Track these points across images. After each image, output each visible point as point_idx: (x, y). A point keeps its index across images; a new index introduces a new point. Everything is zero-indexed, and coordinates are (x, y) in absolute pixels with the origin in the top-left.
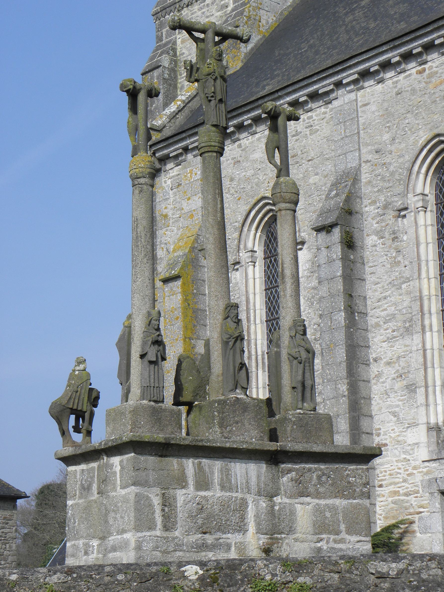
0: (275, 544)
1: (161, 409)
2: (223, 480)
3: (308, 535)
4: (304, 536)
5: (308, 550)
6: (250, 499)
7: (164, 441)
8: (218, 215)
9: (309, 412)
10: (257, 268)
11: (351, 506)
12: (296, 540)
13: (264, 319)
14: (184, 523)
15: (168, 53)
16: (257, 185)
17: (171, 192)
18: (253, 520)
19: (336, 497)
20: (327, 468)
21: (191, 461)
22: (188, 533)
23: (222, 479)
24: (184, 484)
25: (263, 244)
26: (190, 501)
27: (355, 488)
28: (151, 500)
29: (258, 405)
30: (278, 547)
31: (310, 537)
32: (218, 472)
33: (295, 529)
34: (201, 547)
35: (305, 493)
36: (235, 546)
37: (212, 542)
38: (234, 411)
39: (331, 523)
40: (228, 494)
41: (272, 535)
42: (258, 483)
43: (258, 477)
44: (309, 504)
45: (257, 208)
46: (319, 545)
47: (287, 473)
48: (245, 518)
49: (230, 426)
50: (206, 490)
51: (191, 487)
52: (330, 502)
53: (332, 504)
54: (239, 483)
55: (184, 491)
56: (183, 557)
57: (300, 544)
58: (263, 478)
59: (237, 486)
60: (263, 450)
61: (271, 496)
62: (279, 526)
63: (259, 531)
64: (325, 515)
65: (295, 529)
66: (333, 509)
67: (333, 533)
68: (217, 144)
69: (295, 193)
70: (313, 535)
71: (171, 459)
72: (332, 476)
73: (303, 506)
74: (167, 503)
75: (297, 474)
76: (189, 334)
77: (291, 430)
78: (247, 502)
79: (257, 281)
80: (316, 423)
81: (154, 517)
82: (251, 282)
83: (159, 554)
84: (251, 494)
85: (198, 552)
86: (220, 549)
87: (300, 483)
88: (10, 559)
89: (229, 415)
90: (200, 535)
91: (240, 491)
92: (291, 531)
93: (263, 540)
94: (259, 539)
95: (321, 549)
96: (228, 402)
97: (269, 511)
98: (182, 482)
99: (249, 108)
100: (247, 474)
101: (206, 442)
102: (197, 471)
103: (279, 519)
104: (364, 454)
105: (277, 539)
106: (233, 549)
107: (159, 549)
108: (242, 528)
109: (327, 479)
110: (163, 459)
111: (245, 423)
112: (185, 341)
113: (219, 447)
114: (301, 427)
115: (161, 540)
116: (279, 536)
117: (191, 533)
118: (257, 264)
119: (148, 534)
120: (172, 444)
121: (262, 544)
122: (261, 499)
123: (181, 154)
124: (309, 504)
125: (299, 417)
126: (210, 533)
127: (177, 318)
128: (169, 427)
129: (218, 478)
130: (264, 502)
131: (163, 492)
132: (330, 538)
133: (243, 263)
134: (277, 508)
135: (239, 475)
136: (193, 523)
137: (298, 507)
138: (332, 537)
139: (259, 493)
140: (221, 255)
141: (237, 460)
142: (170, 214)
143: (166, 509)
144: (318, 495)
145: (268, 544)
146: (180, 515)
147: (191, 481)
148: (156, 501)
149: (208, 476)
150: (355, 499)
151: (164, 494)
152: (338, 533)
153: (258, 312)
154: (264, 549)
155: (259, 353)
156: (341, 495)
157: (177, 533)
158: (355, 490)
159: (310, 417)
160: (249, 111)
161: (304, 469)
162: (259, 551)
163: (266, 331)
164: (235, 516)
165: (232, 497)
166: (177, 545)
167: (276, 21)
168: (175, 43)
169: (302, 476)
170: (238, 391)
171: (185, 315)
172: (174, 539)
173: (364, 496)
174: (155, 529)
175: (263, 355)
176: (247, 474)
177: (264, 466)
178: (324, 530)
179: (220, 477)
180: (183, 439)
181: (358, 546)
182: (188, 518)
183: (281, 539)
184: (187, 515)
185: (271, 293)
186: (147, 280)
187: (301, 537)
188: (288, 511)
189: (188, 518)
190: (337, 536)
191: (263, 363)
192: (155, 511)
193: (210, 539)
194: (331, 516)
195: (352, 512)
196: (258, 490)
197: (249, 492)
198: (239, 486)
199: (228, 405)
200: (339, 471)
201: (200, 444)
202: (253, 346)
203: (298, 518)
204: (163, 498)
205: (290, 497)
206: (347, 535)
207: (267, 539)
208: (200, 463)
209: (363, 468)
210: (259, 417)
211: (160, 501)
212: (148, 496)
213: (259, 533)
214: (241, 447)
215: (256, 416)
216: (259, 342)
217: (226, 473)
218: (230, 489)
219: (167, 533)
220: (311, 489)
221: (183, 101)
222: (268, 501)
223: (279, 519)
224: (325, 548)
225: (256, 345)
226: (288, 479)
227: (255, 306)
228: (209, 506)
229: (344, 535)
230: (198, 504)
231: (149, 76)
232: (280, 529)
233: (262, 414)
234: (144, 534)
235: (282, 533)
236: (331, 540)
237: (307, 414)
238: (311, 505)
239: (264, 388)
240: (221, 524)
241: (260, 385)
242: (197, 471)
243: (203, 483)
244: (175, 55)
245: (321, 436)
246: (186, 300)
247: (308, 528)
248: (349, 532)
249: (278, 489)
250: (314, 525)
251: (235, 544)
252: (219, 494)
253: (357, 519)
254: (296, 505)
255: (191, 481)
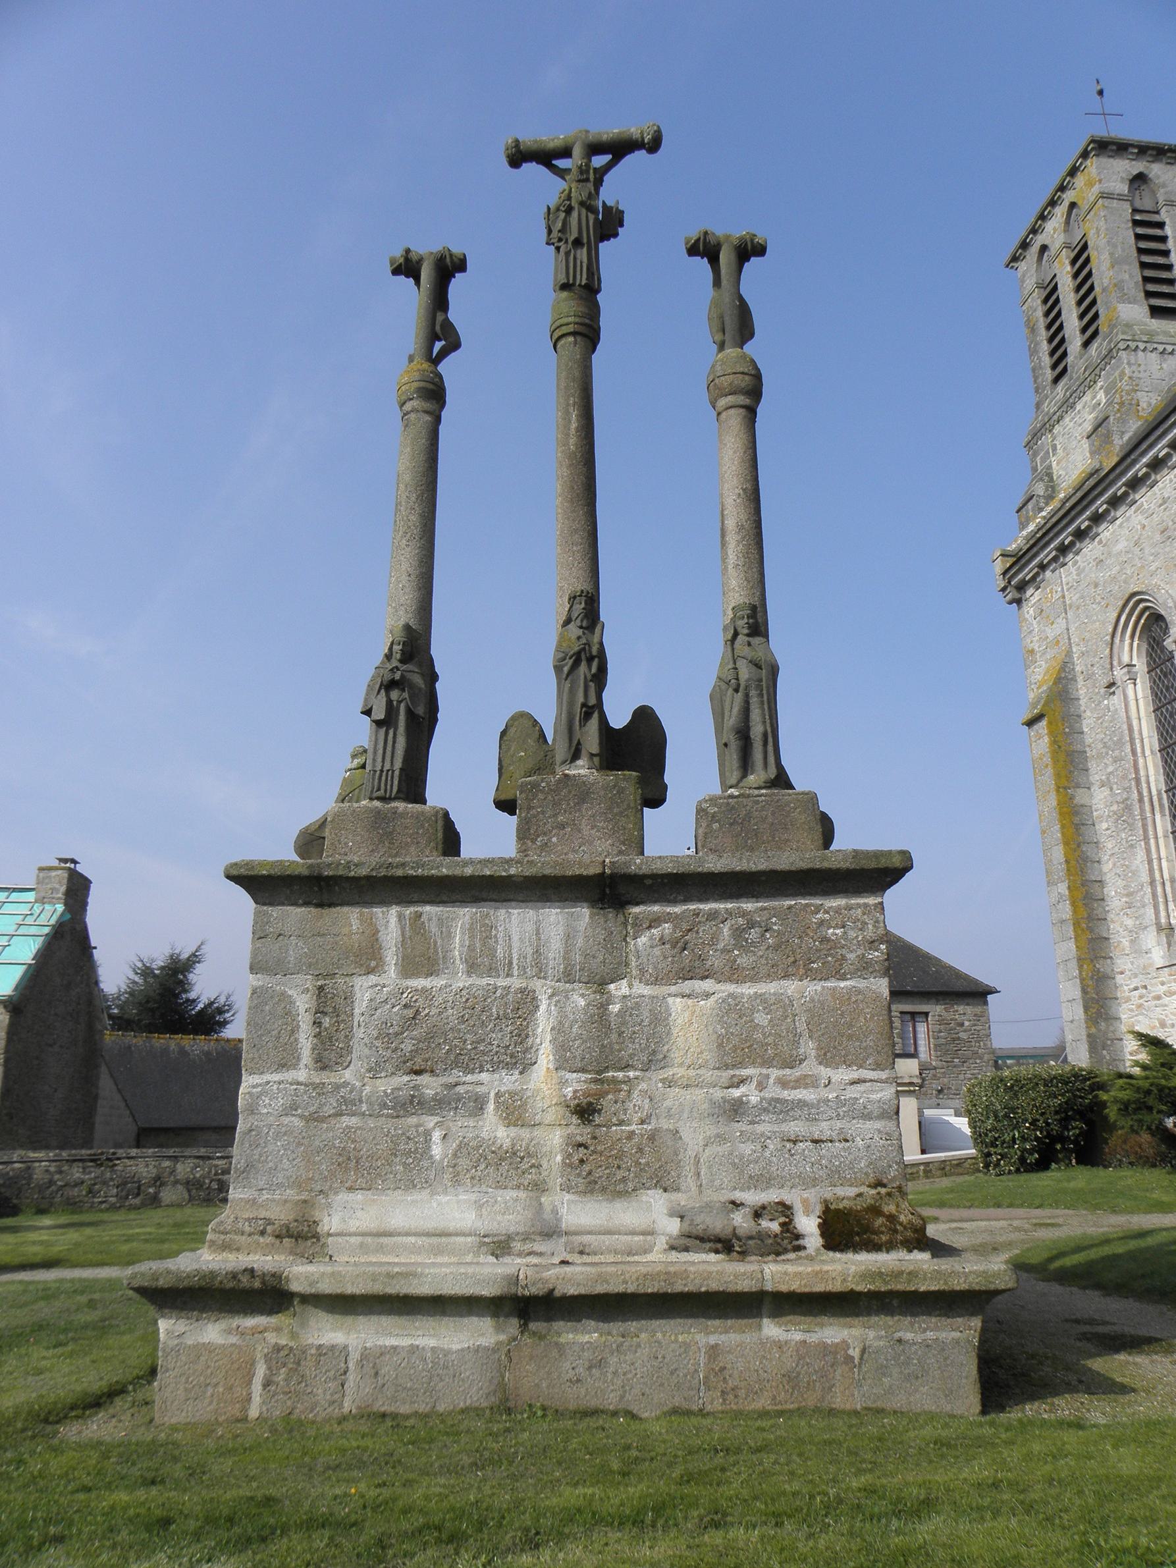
0: (607, 1093)
1: (395, 813)
2: (474, 950)
3: (702, 1071)
4: (692, 1073)
5: (706, 1106)
6: (543, 990)
7: (305, 872)
8: (571, 441)
9: (756, 792)
10: (1139, 686)
11: (833, 997)
12: (669, 1083)
13: (1157, 747)
14: (367, 1051)
15: (1042, 479)
16: (1125, 582)
17: (1035, 622)
18: (549, 1037)
19: (786, 976)
20: (763, 909)
21: (394, 911)
22: (374, 1071)
23: (471, 948)
24: (373, 964)
25: (1144, 654)
26: (386, 1001)
27: (844, 951)
28: (292, 1003)
29: (615, 786)
30: (616, 1102)
31: (708, 1075)
32: (463, 934)
33: (665, 1057)
34: (405, 1104)
35: (697, 971)
36: (496, 1102)
37: (437, 1094)
38: (556, 804)
39: (770, 1040)
40: (484, 981)
41: (599, 1072)
42: (566, 952)
43: (568, 938)
44: (707, 995)
45: (1127, 611)
46: (736, 1093)
47: (650, 927)
48: (527, 1036)
49: (545, 834)
50: (430, 974)
51: (392, 972)
52: (770, 988)
53: (775, 994)
54: (515, 956)
55: (372, 979)
56: (359, 1128)
57: (683, 1092)
58: (580, 942)
59: (510, 963)
60: (564, 877)
61: (601, 983)
62: (619, 1051)
63: (562, 1063)
64: (752, 1021)
65: (665, 1057)
66: (783, 1005)
67: (775, 1063)
68: (571, 319)
69: (743, 373)
70: (718, 1068)
71: (346, 909)
72: (775, 928)
73: (690, 1002)
74: (330, 1006)
75: (675, 927)
76: (1064, 782)
77: (706, 834)
78: (534, 999)
79: (1141, 702)
80: (773, 813)
81: (296, 1040)
82: (1132, 704)
83: (297, 1122)
84: (544, 978)
85: (398, 1117)
86: (457, 1108)
87: (685, 949)
88: (986, 1057)
89: (543, 812)
90: (406, 1078)
91: (516, 973)
92: (654, 1060)
93: (576, 1084)
94: (563, 1083)
95: (742, 1102)
96: (543, 784)
97: (592, 1016)
98: (368, 958)
99: (1099, 489)
100: (538, 933)
101: (413, 868)
102: (408, 934)
103: (620, 1034)
104: (855, 870)
105: (614, 1081)
106: (491, 1106)
107: (300, 1111)
108: (518, 1058)
109: (763, 935)
110: (326, 911)
111: (583, 826)
112: (1058, 791)
113: (447, 876)
114: (731, 824)
115: (305, 1092)
116: (620, 1075)
117: (383, 1074)
118: (1138, 681)
119: (276, 1077)
120: (327, 877)
121: (570, 1095)
122: (573, 990)
123: (1037, 574)
124: (707, 995)
125: (728, 804)
126: (432, 1071)
127: (1047, 766)
128: (412, 849)
129: (462, 946)
130: (583, 995)
131: (319, 983)
132: (768, 1076)
133: (1119, 683)
134: (615, 1008)
135: (515, 938)
136: (389, 1051)
137: (676, 1004)
138: (775, 1073)
139: (568, 977)
140: (574, 511)
141: (513, 904)
142: (1036, 648)
143: (326, 1022)
144: (734, 974)
145: (587, 1094)
146: (359, 1033)
147: (391, 958)
148: (303, 1004)
149: (435, 943)
150: (844, 979)
151: (321, 988)
152: (792, 1062)
153: (1146, 741)
154: (578, 1105)
155: (1154, 792)
156: (802, 971)
157: (348, 1075)
158: (843, 958)
159: (757, 802)
160: (1101, 494)
161: (698, 915)
162: (561, 1110)
163: (1160, 764)
164: (501, 1030)
165: (496, 988)
166: (345, 1101)
167: (1162, 400)
168: (1050, 467)
169: (690, 930)
170: (580, 762)
171: (1055, 761)
172: (337, 1087)
173: (871, 970)
174: (295, 1067)
175: (1159, 794)
176: (538, 933)
177: (583, 914)
178: (749, 1058)
179: (467, 943)
180: (356, 865)
181: (853, 1092)
182: (376, 1038)
183: (628, 1081)
184: (375, 1033)
185: (1162, 713)
186: (405, 577)
187: (683, 1076)
188: (646, 1014)
189: (376, 1038)
190: (788, 1071)
191: (1161, 805)
192: (298, 1026)
193: (430, 1085)
194: (771, 1021)
195: (835, 1009)
196: (565, 968)
197: (541, 973)
198: (515, 962)
199: (542, 791)
200: (796, 915)
201: (400, 873)
202: (1144, 785)
203: (675, 1031)
204: (319, 996)
205: (656, 981)
206: (822, 1068)
207: (585, 1082)
208: (419, 915)
209: (866, 905)
210: (615, 810)
211: (313, 1004)
212: (283, 994)
213: (565, 1069)
214: (504, 874)
215: (610, 809)
216: (1152, 779)
217: (485, 933)
218: (491, 971)
219: (324, 1074)
220: (715, 960)
221: (1044, 517)
222: (595, 992)
223: (620, 1034)
224: (754, 1100)
225: (1148, 783)
226: (651, 938)
227: (1141, 734)
228: (434, 1011)
229: (810, 1067)
230: (405, 1006)
231: (1024, 511)
232: (621, 1059)
233: (626, 803)
234: (267, 1077)
235: (627, 1067)
236: (771, 1081)
237: (749, 796)
238: (712, 999)
239: (1165, 836)
240: (461, 1049)
241: (1160, 834)
242: (408, 934)
243: (422, 958)
244: (1052, 480)
245: (788, 840)
246: (1054, 742)
247: (701, 1053)
248: (825, 1059)
249: (619, 964)
250: (720, 1046)
251: (498, 1095)
252: (462, 981)
253: (851, 1026)
254: (670, 1000)
255: (391, 958)
